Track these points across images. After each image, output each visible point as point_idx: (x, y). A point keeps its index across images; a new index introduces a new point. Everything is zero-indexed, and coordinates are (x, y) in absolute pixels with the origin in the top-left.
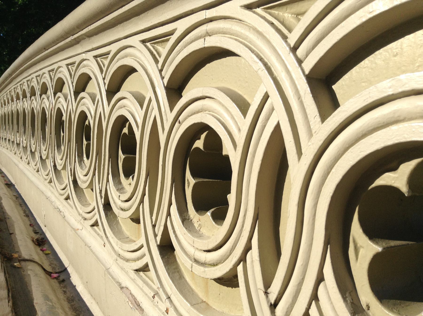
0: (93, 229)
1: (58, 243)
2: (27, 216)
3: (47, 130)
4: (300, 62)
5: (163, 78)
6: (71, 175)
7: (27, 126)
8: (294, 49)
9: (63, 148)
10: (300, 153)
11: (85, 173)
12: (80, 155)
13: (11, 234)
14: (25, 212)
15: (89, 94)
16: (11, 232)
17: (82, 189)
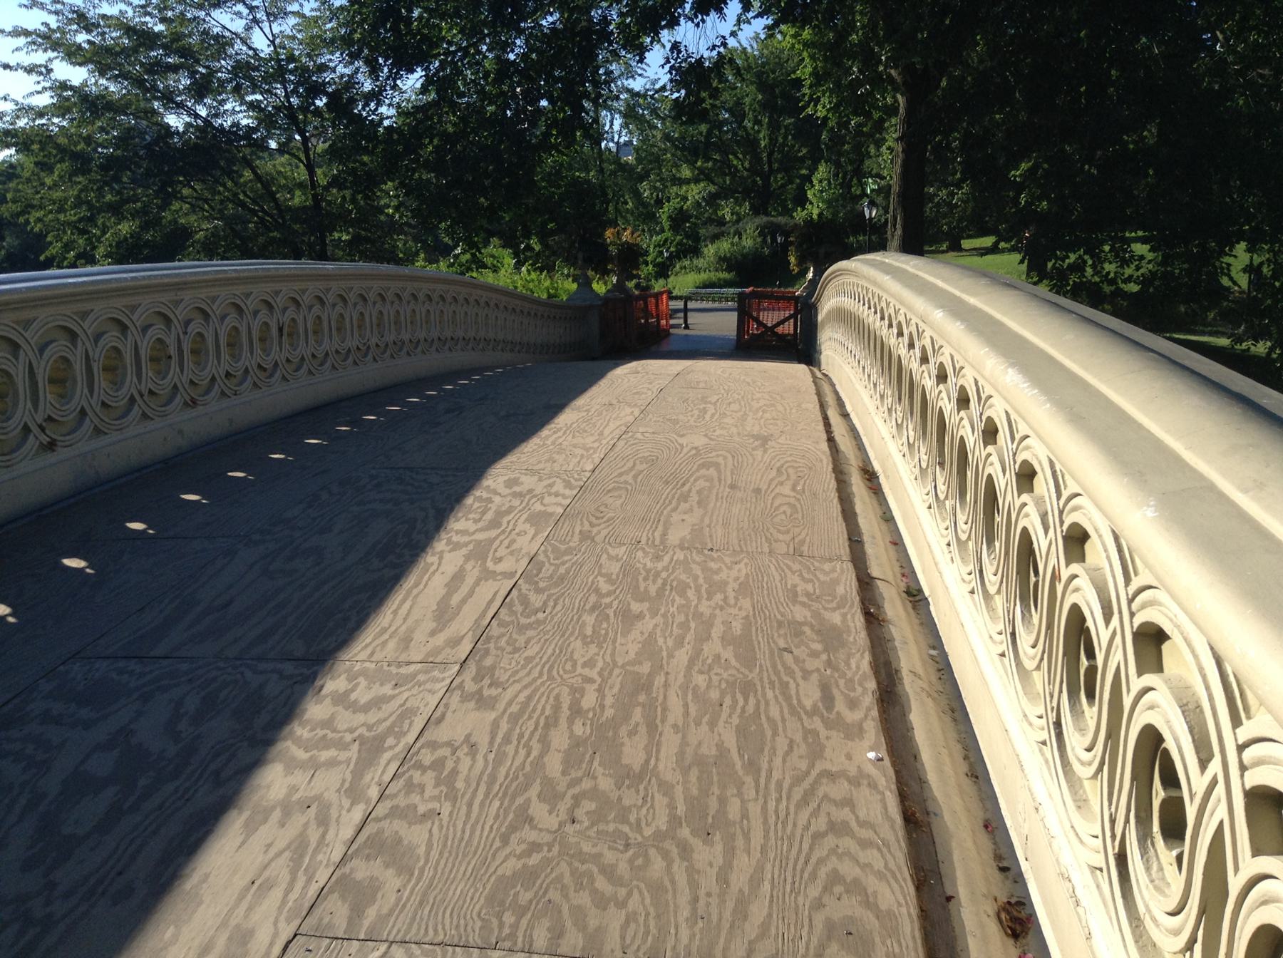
0: (1092, 872)
1: (1049, 914)
2: (1004, 870)
3: (969, 473)
4: (1132, 615)
5: (1062, 522)
6: (1113, 836)
7: (935, 422)
8: (1241, 748)
9: (997, 544)
10: (1128, 691)
11: (1087, 741)
12: (1143, 814)
13: (949, 899)
14: (998, 857)
15: (1167, 681)
16: (949, 893)
17: (1079, 779)
